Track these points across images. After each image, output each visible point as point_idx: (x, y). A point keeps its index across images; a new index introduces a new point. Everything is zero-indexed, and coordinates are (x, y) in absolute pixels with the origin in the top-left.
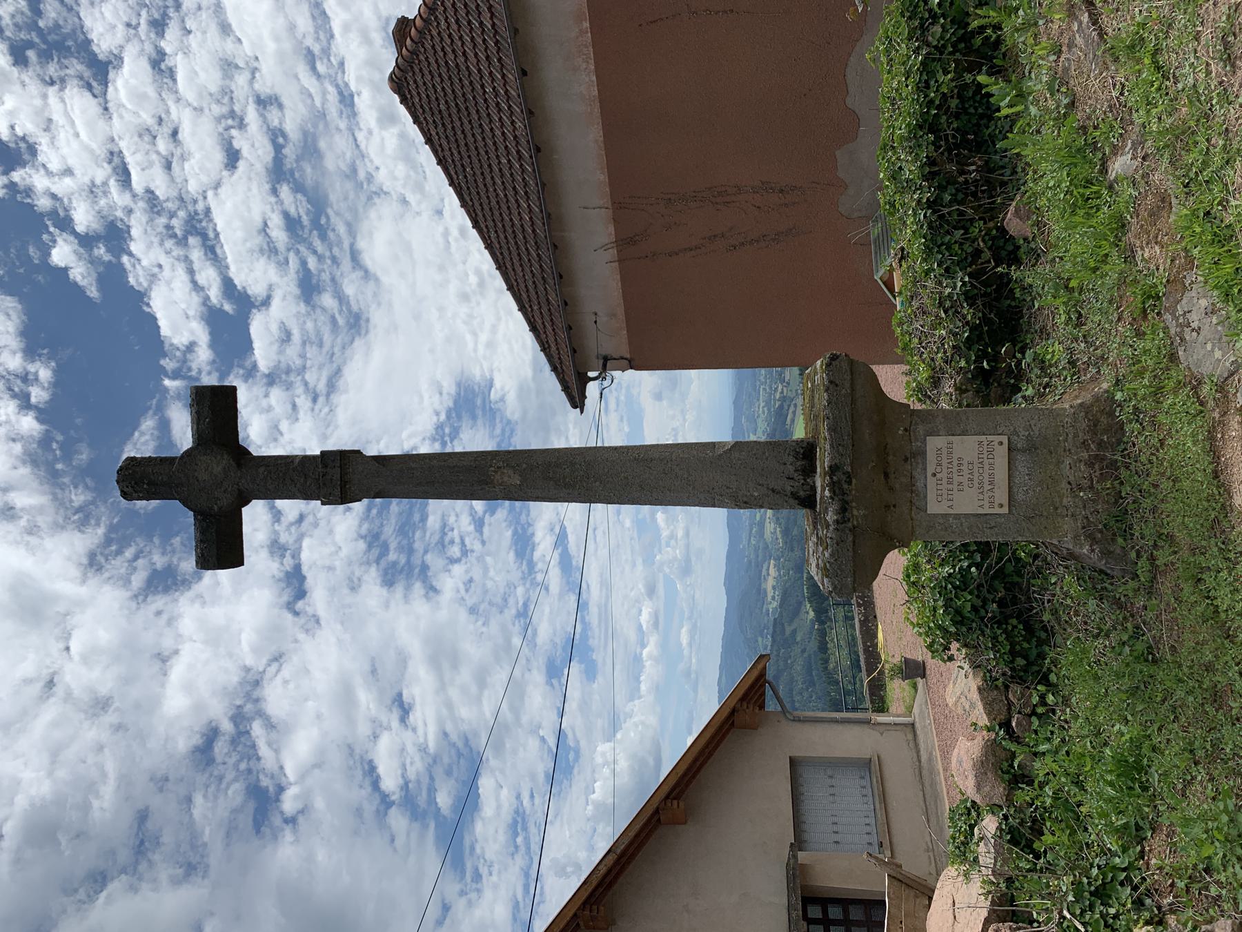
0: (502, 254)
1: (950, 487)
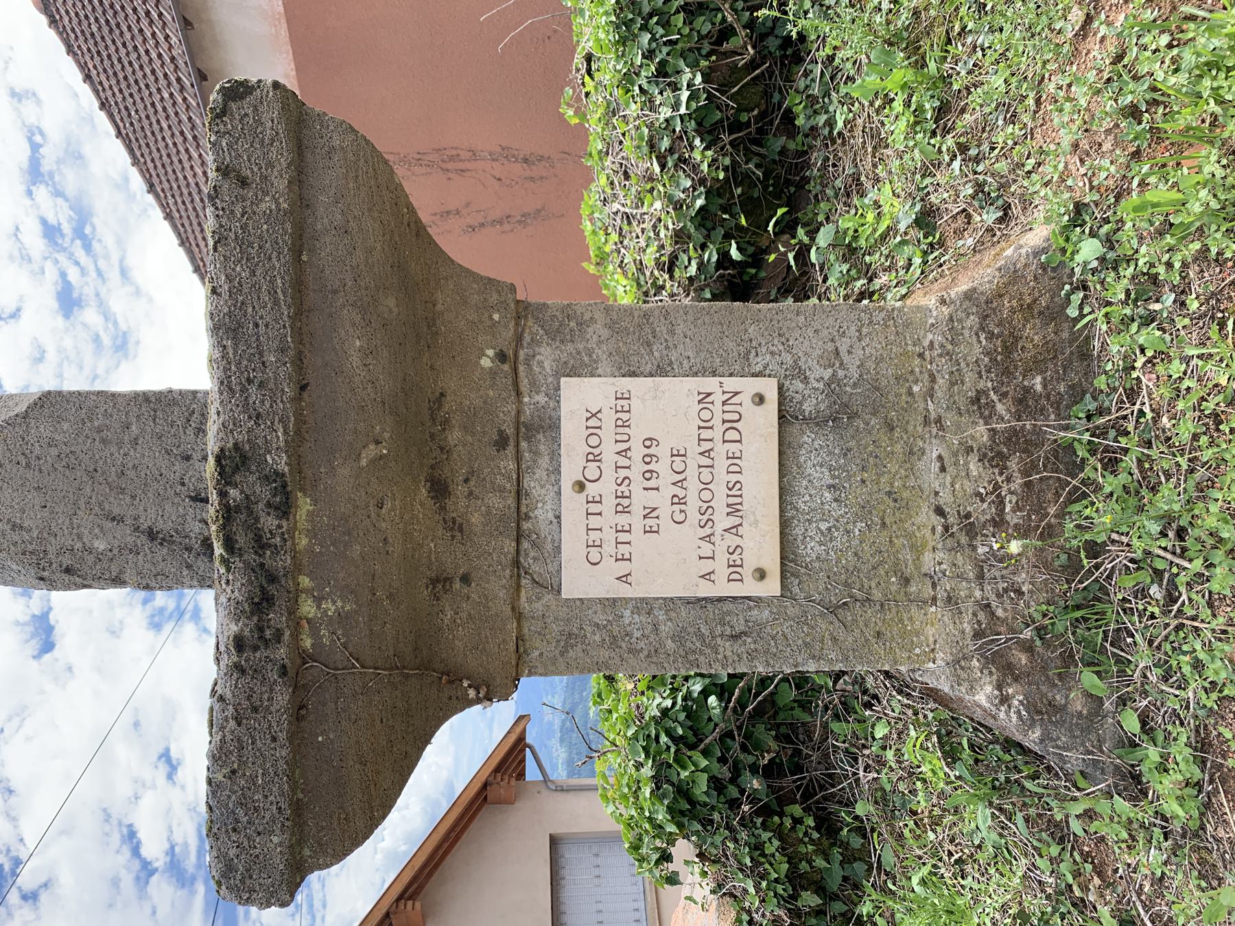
0: (183, 225)
1: (623, 520)
